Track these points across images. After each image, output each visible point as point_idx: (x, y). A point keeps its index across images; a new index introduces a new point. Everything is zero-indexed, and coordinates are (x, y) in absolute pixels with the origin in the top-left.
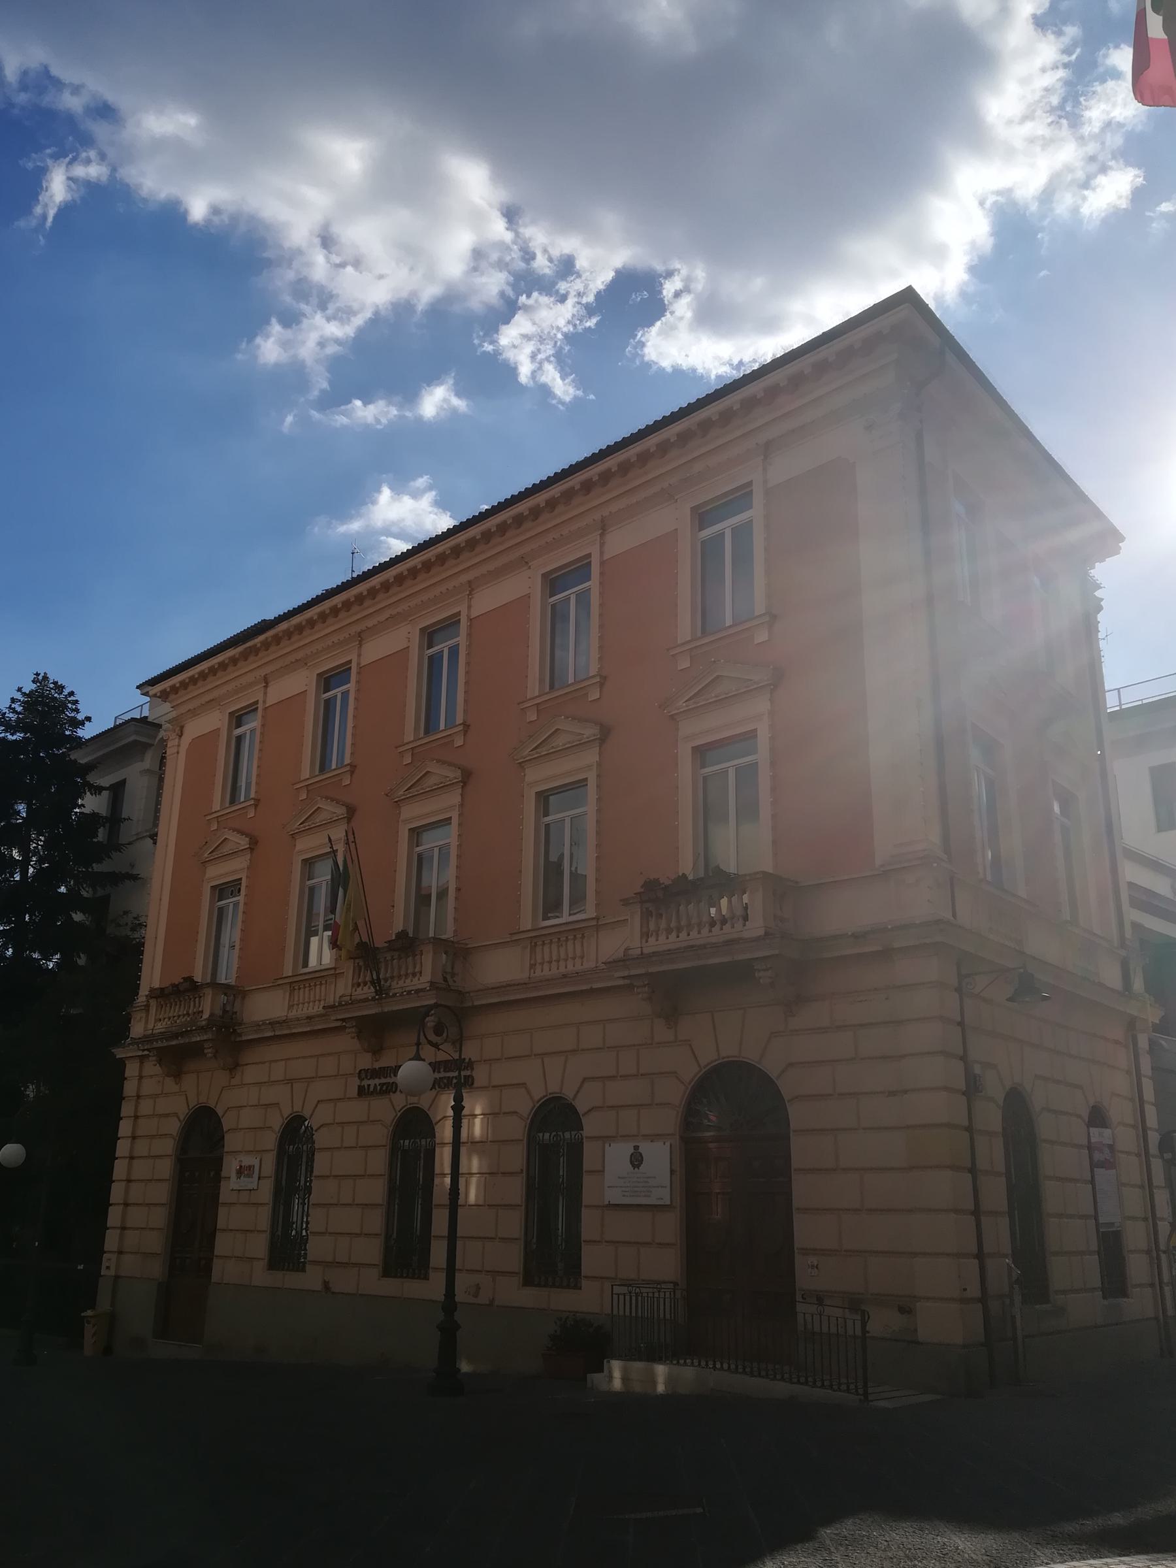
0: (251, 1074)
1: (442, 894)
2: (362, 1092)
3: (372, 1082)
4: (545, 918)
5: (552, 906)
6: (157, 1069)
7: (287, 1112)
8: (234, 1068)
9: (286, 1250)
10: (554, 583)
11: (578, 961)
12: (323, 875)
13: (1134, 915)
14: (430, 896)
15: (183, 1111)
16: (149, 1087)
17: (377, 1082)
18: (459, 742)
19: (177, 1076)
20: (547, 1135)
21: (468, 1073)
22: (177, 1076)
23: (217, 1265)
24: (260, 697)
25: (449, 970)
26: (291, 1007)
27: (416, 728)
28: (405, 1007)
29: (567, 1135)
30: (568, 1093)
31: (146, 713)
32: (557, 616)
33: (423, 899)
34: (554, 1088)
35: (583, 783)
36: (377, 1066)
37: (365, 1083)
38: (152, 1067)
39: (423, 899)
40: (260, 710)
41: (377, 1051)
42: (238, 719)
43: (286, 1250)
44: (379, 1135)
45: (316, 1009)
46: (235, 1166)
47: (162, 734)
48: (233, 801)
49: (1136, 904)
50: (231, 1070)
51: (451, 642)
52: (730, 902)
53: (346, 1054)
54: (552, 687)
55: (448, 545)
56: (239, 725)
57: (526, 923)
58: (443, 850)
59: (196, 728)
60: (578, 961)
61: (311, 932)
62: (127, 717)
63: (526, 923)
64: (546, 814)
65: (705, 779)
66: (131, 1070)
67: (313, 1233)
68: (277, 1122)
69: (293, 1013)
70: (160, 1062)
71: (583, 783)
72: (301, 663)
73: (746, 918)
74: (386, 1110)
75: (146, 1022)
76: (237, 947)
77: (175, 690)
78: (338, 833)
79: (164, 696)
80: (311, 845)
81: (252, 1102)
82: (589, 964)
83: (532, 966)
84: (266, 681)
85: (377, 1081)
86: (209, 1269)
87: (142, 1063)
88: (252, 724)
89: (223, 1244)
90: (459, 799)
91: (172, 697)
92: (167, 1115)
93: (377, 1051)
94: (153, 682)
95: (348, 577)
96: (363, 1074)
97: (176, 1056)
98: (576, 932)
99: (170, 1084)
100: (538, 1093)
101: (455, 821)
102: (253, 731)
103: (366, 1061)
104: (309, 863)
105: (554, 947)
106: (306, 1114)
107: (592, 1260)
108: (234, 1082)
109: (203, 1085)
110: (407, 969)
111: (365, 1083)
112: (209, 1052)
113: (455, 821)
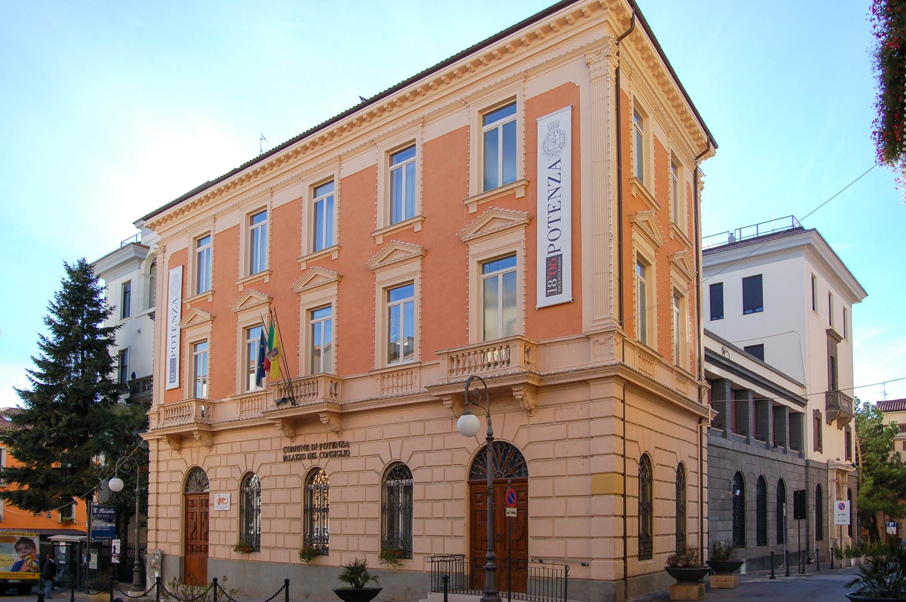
0: (220, 449)
1: (327, 349)
2: (285, 459)
3: (292, 454)
4: (389, 363)
5: (394, 356)
6: (168, 446)
7: (244, 470)
8: (211, 446)
9: (249, 543)
10: (395, 155)
11: (409, 387)
12: (255, 337)
13: (707, 366)
14: (319, 350)
15: (185, 470)
16: (164, 456)
17: (292, 455)
18: (210, 300)
19: (179, 450)
20: (392, 482)
21: (346, 449)
22: (179, 450)
23: (210, 548)
24: (211, 228)
25: (333, 391)
26: (241, 412)
27: (193, 292)
28: (294, 414)
29: (404, 481)
30: (404, 460)
31: (139, 240)
32: (395, 176)
33: (316, 353)
34: (396, 457)
35: (513, 255)
36: (293, 445)
37: (287, 454)
38: (164, 445)
39: (316, 353)
40: (269, 212)
41: (293, 437)
42: (199, 241)
43: (249, 543)
44: (298, 482)
45: (259, 414)
46: (217, 497)
47: (152, 251)
48: (198, 292)
49: (708, 359)
50: (292, 438)
51: (329, 194)
52: (493, 354)
53: (277, 438)
54: (314, 250)
55: (552, 19)
56: (199, 246)
57: (378, 365)
58: (328, 322)
59: (174, 247)
60: (409, 387)
61: (250, 372)
62: (128, 242)
63: (378, 365)
64: (389, 301)
65: (313, 325)
66: (152, 446)
67: (264, 533)
68: (239, 476)
69: (244, 417)
70: (169, 442)
71: (513, 255)
72: (236, 207)
73: (509, 362)
74: (301, 468)
75: (159, 419)
76: (333, 348)
77: (159, 223)
78: (265, 310)
79: (153, 227)
80: (245, 318)
81: (223, 466)
82: (416, 389)
83: (382, 389)
84: (215, 218)
85: (294, 453)
86: (206, 551)
87: (158, 442)
88: (208, 245)
89: (213, 538)
90: (336, 292)
91: (157, 227)
92: (175, 471)
93: (293, 437)
94: (146, 218)
95: (257, 154)
96: (286, 449)
97: (179, 440)
98: (407, 370)
99: (175, 454)
100: (387, 460)
101: (334, 305)
102: (208, 249)
103: (287, 443)
104: (248, 330)
105: (395, 379)
106: (255, 470)
107: (417, 545)
108: (212, 453)
109: (194, 455)
110: (470, 364)
111: (287, 454)
112: (197, 437)
113: (334, 305)
